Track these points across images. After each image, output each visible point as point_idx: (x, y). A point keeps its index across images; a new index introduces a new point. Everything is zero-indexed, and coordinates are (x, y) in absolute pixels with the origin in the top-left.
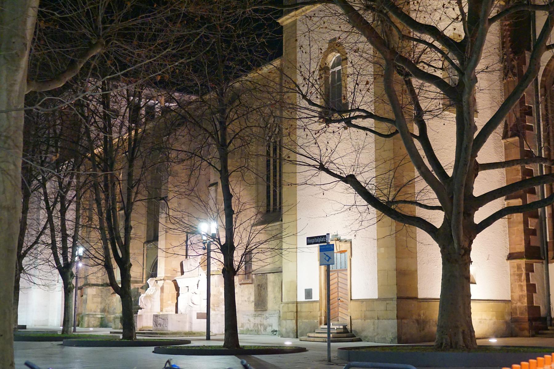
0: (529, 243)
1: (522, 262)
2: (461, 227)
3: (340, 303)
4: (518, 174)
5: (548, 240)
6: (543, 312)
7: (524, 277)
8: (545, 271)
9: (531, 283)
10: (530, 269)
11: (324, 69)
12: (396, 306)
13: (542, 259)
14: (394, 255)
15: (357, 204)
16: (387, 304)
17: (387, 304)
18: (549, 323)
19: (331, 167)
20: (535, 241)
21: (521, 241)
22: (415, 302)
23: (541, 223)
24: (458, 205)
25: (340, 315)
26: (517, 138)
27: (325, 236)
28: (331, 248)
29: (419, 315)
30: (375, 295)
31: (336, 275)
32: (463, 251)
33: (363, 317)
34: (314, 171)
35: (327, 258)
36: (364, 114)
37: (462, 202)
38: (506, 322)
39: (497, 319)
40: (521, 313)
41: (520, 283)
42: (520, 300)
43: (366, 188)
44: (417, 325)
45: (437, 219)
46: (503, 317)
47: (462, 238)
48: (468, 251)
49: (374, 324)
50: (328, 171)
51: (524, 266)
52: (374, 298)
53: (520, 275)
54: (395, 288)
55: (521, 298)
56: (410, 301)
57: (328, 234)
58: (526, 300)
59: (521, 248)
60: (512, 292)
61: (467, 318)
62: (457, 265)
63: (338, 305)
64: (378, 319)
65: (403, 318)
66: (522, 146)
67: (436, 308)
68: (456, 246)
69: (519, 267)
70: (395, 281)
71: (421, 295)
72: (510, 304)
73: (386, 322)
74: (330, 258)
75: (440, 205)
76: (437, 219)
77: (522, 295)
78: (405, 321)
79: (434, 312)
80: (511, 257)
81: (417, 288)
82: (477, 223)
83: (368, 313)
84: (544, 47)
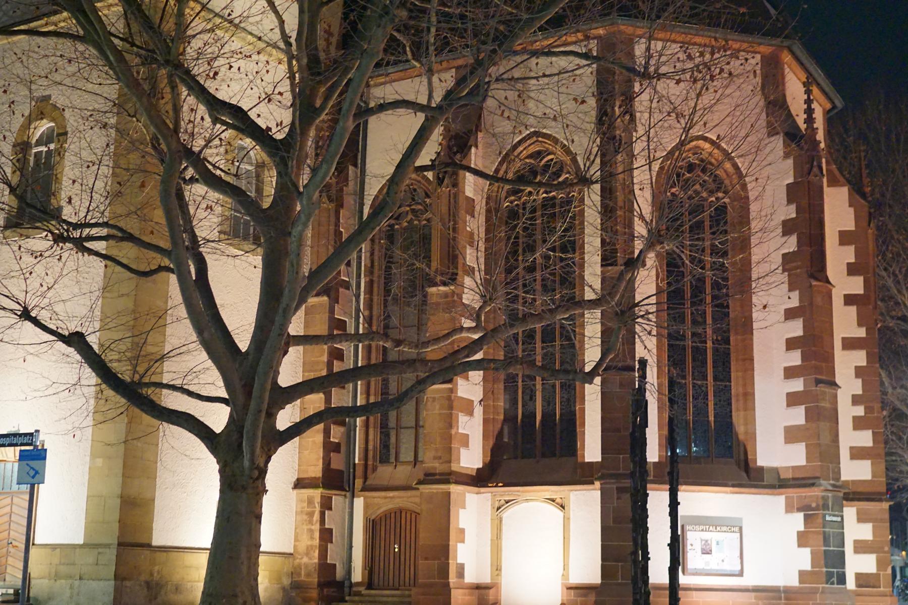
0: (329, 464)
1: (317, 494)
2: (260, 434)
3: (11, 550)
4: (322, 355)
5: (357, 461)
6: (340, 574)
7: (317, 516)
8: (347, 510)
9: (327, 526)
10: (326, 505)
11: (23, 147)
12: (114, 558)
13: (344, 490)
14: (119, 470)
15: (83, 382)
16: (99, 553)
17: (99, 553)
18: (347, 590)
19: (44, 316)
20: (338, 462)
21: (318, 460)
22: (146, 552)
23: (349, 436)
24: (261, 397)
25: (9, 570)
26: (325, 298)
27: (31, 434)
28: (40, 455)
29: (152, 575)
30: (79, 539)
31: (8, 500)
32: (256, 473)
33: (53, 574)
34: (13, 319)
35: (32, 473)
36: (120, 235)
37: (267, 394)
38: (284, 589)
39: (270, 581)
40: (308, 575)
41: (309, 527)
42: (307, 554)
43: (103, 357)
44: (146, 590)
45: (217, 418)
46: (279, 579)
47: (258, 450)
48: (263, 472)
49: (71, 587)
50: (36, 322)
51: (319, 500)
52: (77, 543)
53: (311, 514)
54: (116, 526)
55: (309, 549)
56: (138, 550)
57: (38, 431)
58: (316, 554)
59: (316, 470)
60: (296, 540)
61: (252, 582)
62: (244, 496)
63: (8, 552)
64: (81, 579)
65: (124, 579)
66: (332, 311)
67: (202, 562)
68: (246, 463)
69: (310, 501)
70: (116, 516)
71: (156, 541)
72: (291, 560)
73: (94, 584)
74: (37, 473)
75: (225, 395)
76: (217, 418)
77: (311, 546)
78: (128, 583)
79: (195, 573)
80: (299, 484)
81: (152, 529)
82: (281, 430)
83: (63, 569)
84: (412, 168)
